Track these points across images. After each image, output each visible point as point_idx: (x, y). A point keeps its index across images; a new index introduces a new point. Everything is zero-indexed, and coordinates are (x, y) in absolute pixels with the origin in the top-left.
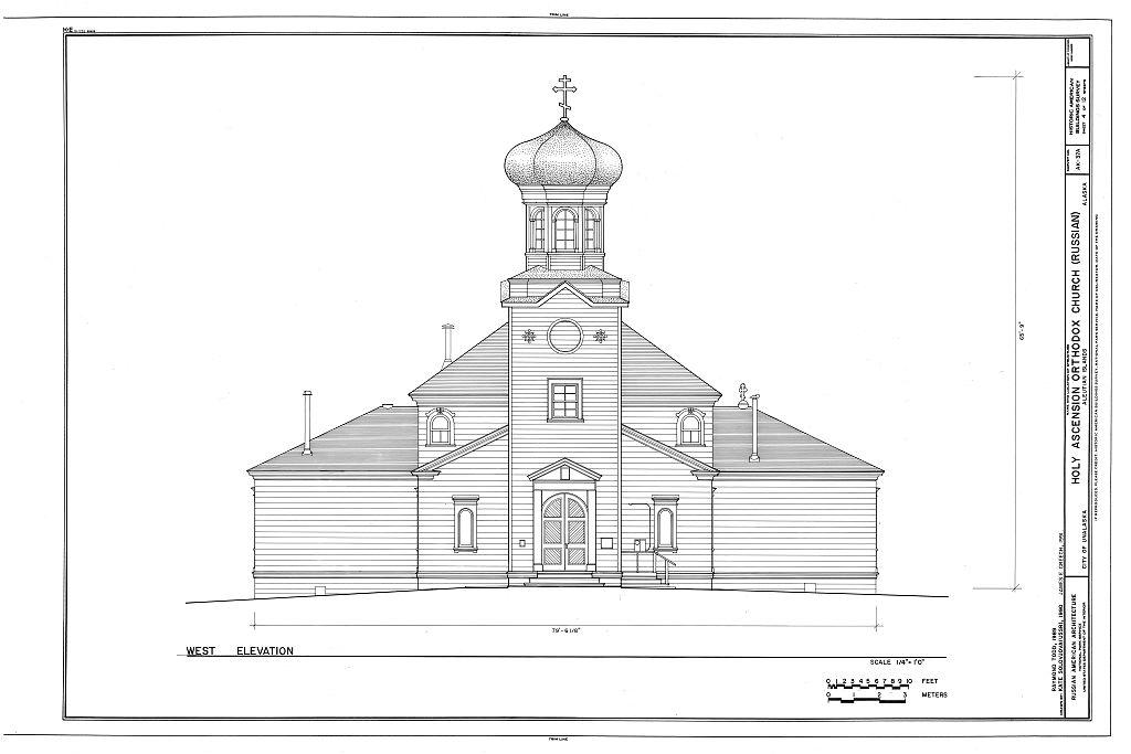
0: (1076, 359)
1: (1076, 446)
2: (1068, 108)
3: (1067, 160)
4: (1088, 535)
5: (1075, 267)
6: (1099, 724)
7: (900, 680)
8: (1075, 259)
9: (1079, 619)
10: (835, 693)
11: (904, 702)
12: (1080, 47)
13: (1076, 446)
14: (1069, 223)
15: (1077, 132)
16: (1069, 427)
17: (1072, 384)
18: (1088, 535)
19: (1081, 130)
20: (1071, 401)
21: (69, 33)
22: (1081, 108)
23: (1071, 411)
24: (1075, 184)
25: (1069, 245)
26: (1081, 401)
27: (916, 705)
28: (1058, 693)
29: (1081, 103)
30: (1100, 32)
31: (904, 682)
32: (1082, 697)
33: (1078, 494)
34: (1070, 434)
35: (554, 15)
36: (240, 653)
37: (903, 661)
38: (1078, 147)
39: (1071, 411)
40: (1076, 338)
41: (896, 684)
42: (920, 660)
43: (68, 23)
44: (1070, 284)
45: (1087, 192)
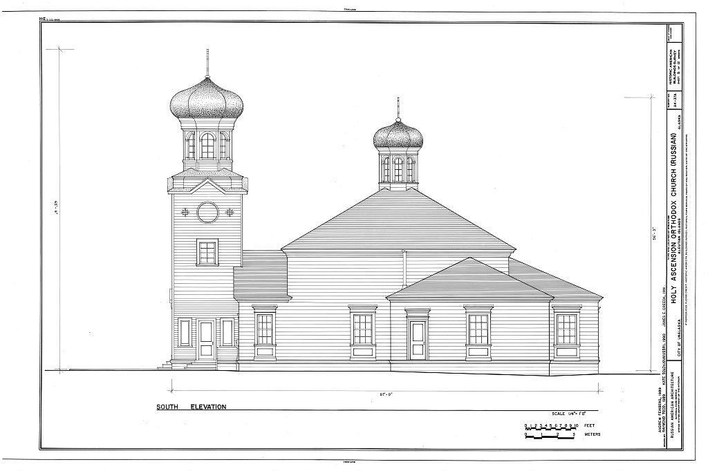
0: (673, 225)
1: (674, 279)
2: (669, 68)
3: (668, 101)
4: (681, 335)
5: (674, 168)
6: (688, 453)
7: (571, 425)
8: (673, 162)
9: (676, 387)
10: (530, 433)
11: (573, 438)
12: (676, 30)
13: (674, 279)
14: (670, 140)
15: (674, 82)
16: (669, 267)
17: (671, 240)
18: (681, 335)
19: (677, 82)
20: (670, 251)
21: (43, 21)
22: (677, 68)
23: (670, 257)
24: (673, 115)
25: (669, 154)
26: (677, 251)
27: (580, 441)
28: (662, 434)
29: (677, 65)
30: (688, 20)
31: (573, 426)
32: (678, 436)
33: (674, 311)
34: (670, 272)
35: (347, 10)
36: (193, 408)
37: (573, 412)
38: (675, 93)
39: (670, 257)
40: (674, 212)
41: (568, 427)
42: (584, 412)
43: (42, 15)
44: (670, 178)
45: (681, 120)
